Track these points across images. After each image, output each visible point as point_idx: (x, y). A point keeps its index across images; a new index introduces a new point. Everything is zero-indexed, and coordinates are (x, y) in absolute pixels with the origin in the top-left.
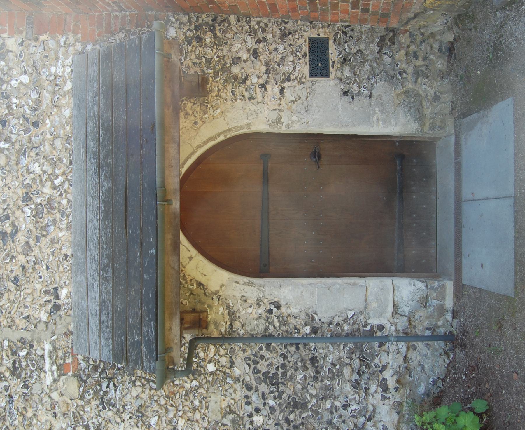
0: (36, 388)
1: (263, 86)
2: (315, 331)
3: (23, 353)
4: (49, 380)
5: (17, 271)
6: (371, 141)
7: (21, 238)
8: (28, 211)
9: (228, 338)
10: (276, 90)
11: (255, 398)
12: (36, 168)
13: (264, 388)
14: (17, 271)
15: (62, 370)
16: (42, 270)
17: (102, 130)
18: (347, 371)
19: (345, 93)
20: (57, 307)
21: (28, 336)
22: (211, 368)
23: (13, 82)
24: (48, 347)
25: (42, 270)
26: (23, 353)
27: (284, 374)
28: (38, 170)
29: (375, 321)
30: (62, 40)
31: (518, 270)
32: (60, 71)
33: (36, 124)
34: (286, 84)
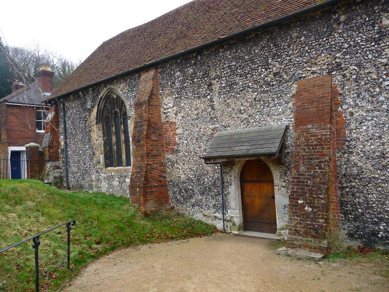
0: (209, 124)
1: (284, 181)
2: (226, 195)
3: (215, 120)
4: (210, 127)
5: (233, 116)
6: (7, 170)
7: (240, 115)
8: (246, 117)
9: (222, 173)
10: (284, 185)
11: (211, 179)
12: (257, 117)
13: (213, 181)
14: (233, 116)
15: (213, 130)
16: (233, 122)
17: (135, 157)
18: (217, 203)
19: (285, 206)
20: (225, 127)
21: (219, 120)
22: (216, 168)
23: (279, 107)
24: (217, 126)
25: (233, 122)
26: (215, 120)
27: (216, 187)
28: (256, 118)
29: (229, 211)
30: (292, 120)
31: (29, 171)
32: (283, 120)
33: (268, 115)
34: (286, 188)
